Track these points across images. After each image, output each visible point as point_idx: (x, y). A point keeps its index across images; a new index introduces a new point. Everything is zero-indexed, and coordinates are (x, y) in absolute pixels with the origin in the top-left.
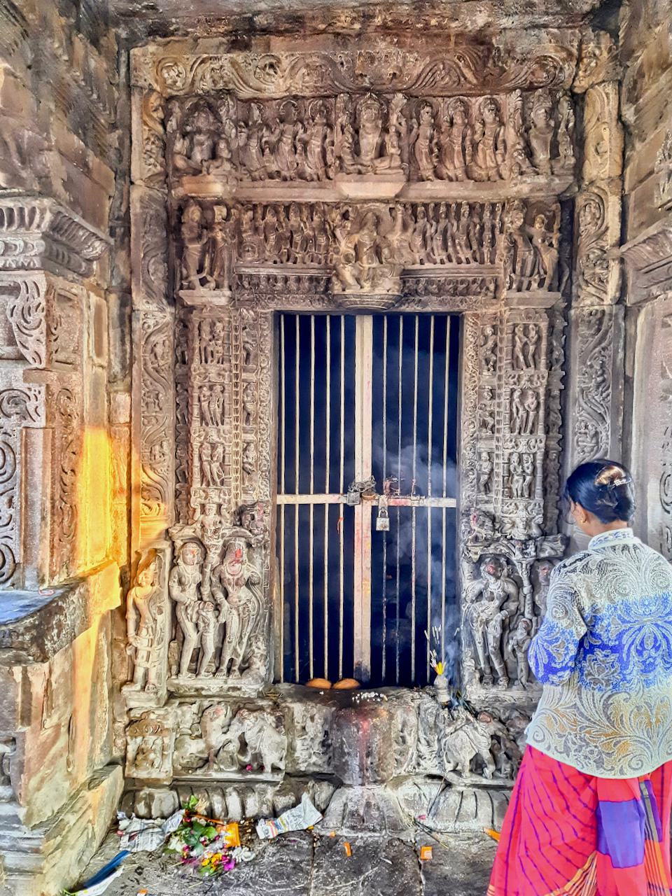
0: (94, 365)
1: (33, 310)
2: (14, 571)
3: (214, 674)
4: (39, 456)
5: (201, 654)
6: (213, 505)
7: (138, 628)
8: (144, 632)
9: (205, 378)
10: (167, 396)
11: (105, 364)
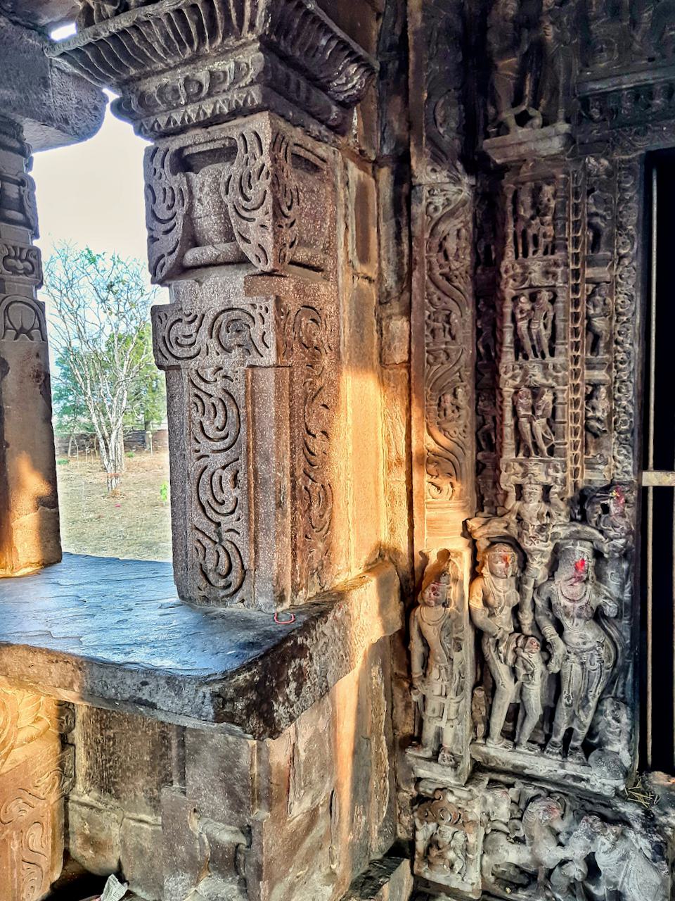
0: (355, 274)
1: (254, 177)
2: (243, 580)
3: (543, 747)
4: (270, 409)
5: (521, 714)
6: (535, 481)
7: (425, 666)
8: (434, 673)
9: (523, 282)
10: (463, 318)
11: (374, 276)
